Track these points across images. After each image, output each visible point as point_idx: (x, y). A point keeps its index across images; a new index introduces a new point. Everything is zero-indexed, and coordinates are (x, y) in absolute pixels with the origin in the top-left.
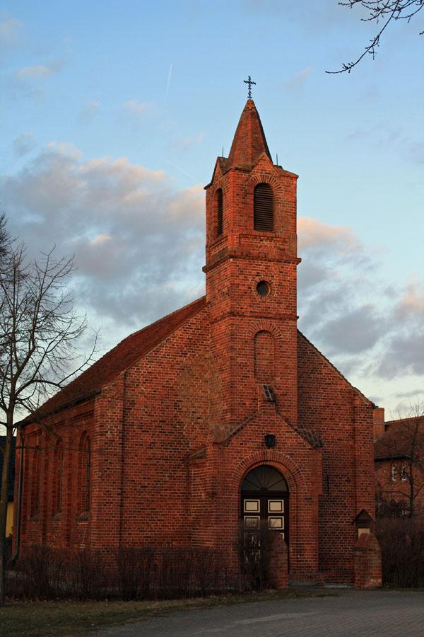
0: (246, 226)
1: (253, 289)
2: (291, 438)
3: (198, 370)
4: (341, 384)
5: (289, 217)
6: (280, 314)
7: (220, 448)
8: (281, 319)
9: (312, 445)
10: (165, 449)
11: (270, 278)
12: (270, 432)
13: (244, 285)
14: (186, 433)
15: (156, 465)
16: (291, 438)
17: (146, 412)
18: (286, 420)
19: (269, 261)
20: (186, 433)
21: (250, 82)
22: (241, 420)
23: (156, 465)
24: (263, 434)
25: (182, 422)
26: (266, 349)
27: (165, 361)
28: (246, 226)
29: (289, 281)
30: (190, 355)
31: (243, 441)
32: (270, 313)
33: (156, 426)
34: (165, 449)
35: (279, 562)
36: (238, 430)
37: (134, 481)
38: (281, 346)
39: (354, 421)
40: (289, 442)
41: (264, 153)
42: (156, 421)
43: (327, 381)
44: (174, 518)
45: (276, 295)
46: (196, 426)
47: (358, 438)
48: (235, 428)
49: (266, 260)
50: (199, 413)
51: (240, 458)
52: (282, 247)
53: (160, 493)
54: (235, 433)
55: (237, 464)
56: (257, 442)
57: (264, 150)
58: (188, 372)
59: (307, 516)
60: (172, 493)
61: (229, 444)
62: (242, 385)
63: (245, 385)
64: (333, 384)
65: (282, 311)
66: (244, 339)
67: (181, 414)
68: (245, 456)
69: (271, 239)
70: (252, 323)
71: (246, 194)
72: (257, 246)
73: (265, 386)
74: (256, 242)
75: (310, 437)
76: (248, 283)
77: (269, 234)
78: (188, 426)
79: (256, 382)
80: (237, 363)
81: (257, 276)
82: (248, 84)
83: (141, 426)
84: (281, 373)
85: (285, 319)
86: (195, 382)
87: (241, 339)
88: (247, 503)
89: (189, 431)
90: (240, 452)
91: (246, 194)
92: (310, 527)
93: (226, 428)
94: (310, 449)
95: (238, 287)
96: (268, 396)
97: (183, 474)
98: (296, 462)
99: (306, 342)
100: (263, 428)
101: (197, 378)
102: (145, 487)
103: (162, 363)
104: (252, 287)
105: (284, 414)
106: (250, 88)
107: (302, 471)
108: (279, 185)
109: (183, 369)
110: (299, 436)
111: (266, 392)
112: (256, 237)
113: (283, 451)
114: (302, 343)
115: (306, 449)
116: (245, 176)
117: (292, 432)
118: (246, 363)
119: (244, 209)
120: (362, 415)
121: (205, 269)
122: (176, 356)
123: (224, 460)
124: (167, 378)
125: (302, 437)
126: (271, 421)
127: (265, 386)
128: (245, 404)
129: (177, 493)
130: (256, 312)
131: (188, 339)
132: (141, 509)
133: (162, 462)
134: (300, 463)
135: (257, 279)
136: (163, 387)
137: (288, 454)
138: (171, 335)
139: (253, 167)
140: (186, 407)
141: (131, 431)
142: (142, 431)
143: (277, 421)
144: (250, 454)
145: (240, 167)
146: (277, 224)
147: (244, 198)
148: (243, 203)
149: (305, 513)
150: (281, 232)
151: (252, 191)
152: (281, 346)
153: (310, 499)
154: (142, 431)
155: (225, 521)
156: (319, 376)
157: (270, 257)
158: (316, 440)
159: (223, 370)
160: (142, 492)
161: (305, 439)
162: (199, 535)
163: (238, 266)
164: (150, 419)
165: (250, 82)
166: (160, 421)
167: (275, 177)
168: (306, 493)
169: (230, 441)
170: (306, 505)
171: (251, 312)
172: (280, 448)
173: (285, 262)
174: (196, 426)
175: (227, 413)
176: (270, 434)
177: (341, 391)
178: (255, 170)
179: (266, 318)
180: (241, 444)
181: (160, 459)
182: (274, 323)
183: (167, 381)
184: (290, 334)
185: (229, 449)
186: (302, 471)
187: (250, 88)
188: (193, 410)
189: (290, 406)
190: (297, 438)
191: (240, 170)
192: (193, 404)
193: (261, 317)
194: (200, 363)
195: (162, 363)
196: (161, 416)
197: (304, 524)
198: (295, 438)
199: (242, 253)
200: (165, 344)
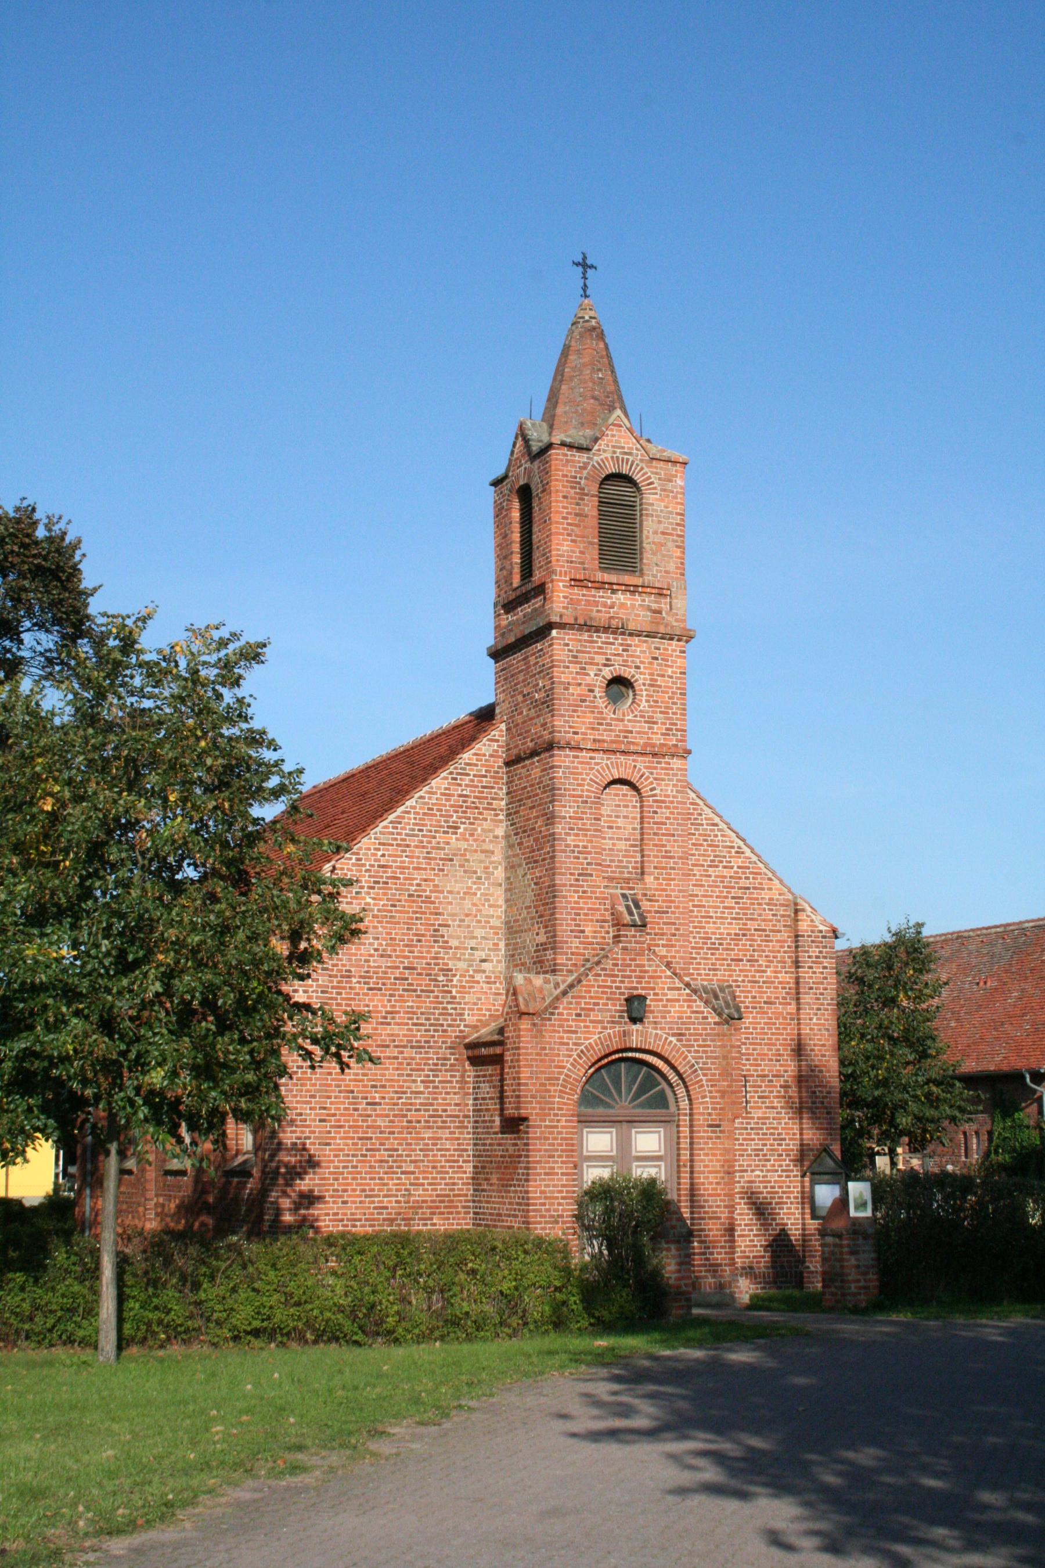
0: (583, 563)
1: (599, 692)
2: (678, 1001)
3: (481, 862)
4: (770, 889)
5: (670, 544)
6: (653, 745)
7: (534, 1025)
8: (654, 755)
9: (720, 1015)
10: (415, 1024)
11: (633, 671)
12: (636, 988)
13: (580, 684)
14: (457, 992)
15: (396, 1058)
16: (678, 1001)
17: (376, 950)
18: (668, 965)
19: (631, 635)
20: (457, 992)
21: (584, 265)
22: (575, 965)
23: (396, 1058)
24: (621, 994)
25: (451, 970)
26: (625, 817)
27: (413, 842)
28: (583, 563)
29: (671, 677)
30: (465, 829)
31: (582, 1009)
32: (633, 743)
33: (395, 979)
34: (415, 1024)
35: (472, 1215)
36: (571, 986)
37: (352, 1092)
38: (655, 812)
39: (797, 964)
40: (674, 1010)
41: (618, 412)
42: (398, 968)
43: (743, 883)
44: (434, 1167)
45: (644, 703)
46: (478, 977)
47: (806, 999)
48: (564, 982)
49: (623, 634)
50: (483, 950)
51: (575, 1044)
52: (654, 606)
53: (406, 1116)
54: (565, 993)
55: (570, 1056)
56: (610, 1011)
57: (617, 405)
58: (461, 866)
59: (711, 1161)
60: (430, 1116)
61: (553, 1014)
62: (577, 892)
63: (584, 892)
64: (755, 888)
65: (658, 740)
66: (581, 796)
67: (447, 953)
68: (586, 1039)
69: (633, 590)
70: (597, 764)
71: (583, 494)
72: (605, 605)
73: (624, 896)
74: (603, 596)
75: (716, 997)
76: (588, 680)
77: (627, 579)
78: (461, 976)
79: (606, 887)
80: (567, 846)
81: (605, 665)
82: (580, 269)
83: (366, 977)
84: (655, 868)
85: (664, 756)
86: (475, 887)
87: (574, 796)
88: (590, 1136)
89: (464, 987)
90: (575, 1032)
91: (583, 494)
92: (717, 1183)
93: (547, 981)
94: (715, 1023)
95: (567, 689)
96: (631, 913)
97: (452, 1076)
98: (690, 1052)
99: (436, 741)
100: (622, 982)
101: (479, 878)
102: (375, 1104)
103: (408, 846)
104: (597, 689)
105: (663, 951)
106: (585, 278)
107: (702, 1069)
108: (649, 478)
109: (451, 860)
110: (694, 997)
111: (628, 907)
112: (601, 585)
113: (661, 1029)
114: (691, 804)
115: (709, 1024)
116: (581, 457)
117: (679, 989)
118: (585, 847)
119: (577, 526)
120: (814, 951)
121: (497, 654)
122: (436, 831)
123: (544, 1049)
124: (418, 876)
125: (701, 998)
126: (637, 966)
127: (624, 896)
128: (583, 931)
129: (441, 1116)
130: (604, 741)
131: (460, 796)
132: (367, 1150)
133: (408, 1052)
134: (697, 1052)
135: (608, 673)
136: (410, 895)
137: (674, 1035)
138: (426, 788)
139: (596, 440)
140: (458, 937)
141: (344, 988)
142: (370, 989)
143: (650, 966)
144: (596, 1037)
145: (568, 440)
146: (648, 557)
147: (578, 504)
148: (576, 515)
149: (707, 1155)
150: (654, 576)
151: (594, 489)
152: (655, 812)
153: (718, 1126)
154: (370, 989)
155: (546, 1174)
156: (725, 872)
157: (631, 626)
158: (728, 1006)
159: (536, 862)
160: (370, 1116)
161: (707, 1002)
162: (488, 1202)
163: (568, 645)
164: (384, 963)
165: (584, 265)
166: (405, 968)
167: (642, 461)
168: (710, 1114)
169: (556, 1008)
170: (710, 1138)
171: (594, 740)
172: (655, 1023)
173: (662, 638)
174: (478, 977)
175: (545, 950)
176: (635, 992)
177: (771, 902)
178: (602, 444)
179: (623, 752)
180: (578, 1015)
181: (405, 1047)
182: (641, 763)
183: (418, 885)
184: (674, 785)
185: (554, 1025)
186: (702, 1069)
187: (585, 278)
188: (473, 943)
189: (674, 935)
190: (690, 1001)
191: (571, 446)
192: (472, 932)
193: (614, 752)
194: (485, 847)
195: (408, 846)
196: (408, 957)
197: (708, 1178)
198: (684, 1001)
199: (576, 619)
200: (414, 808)
